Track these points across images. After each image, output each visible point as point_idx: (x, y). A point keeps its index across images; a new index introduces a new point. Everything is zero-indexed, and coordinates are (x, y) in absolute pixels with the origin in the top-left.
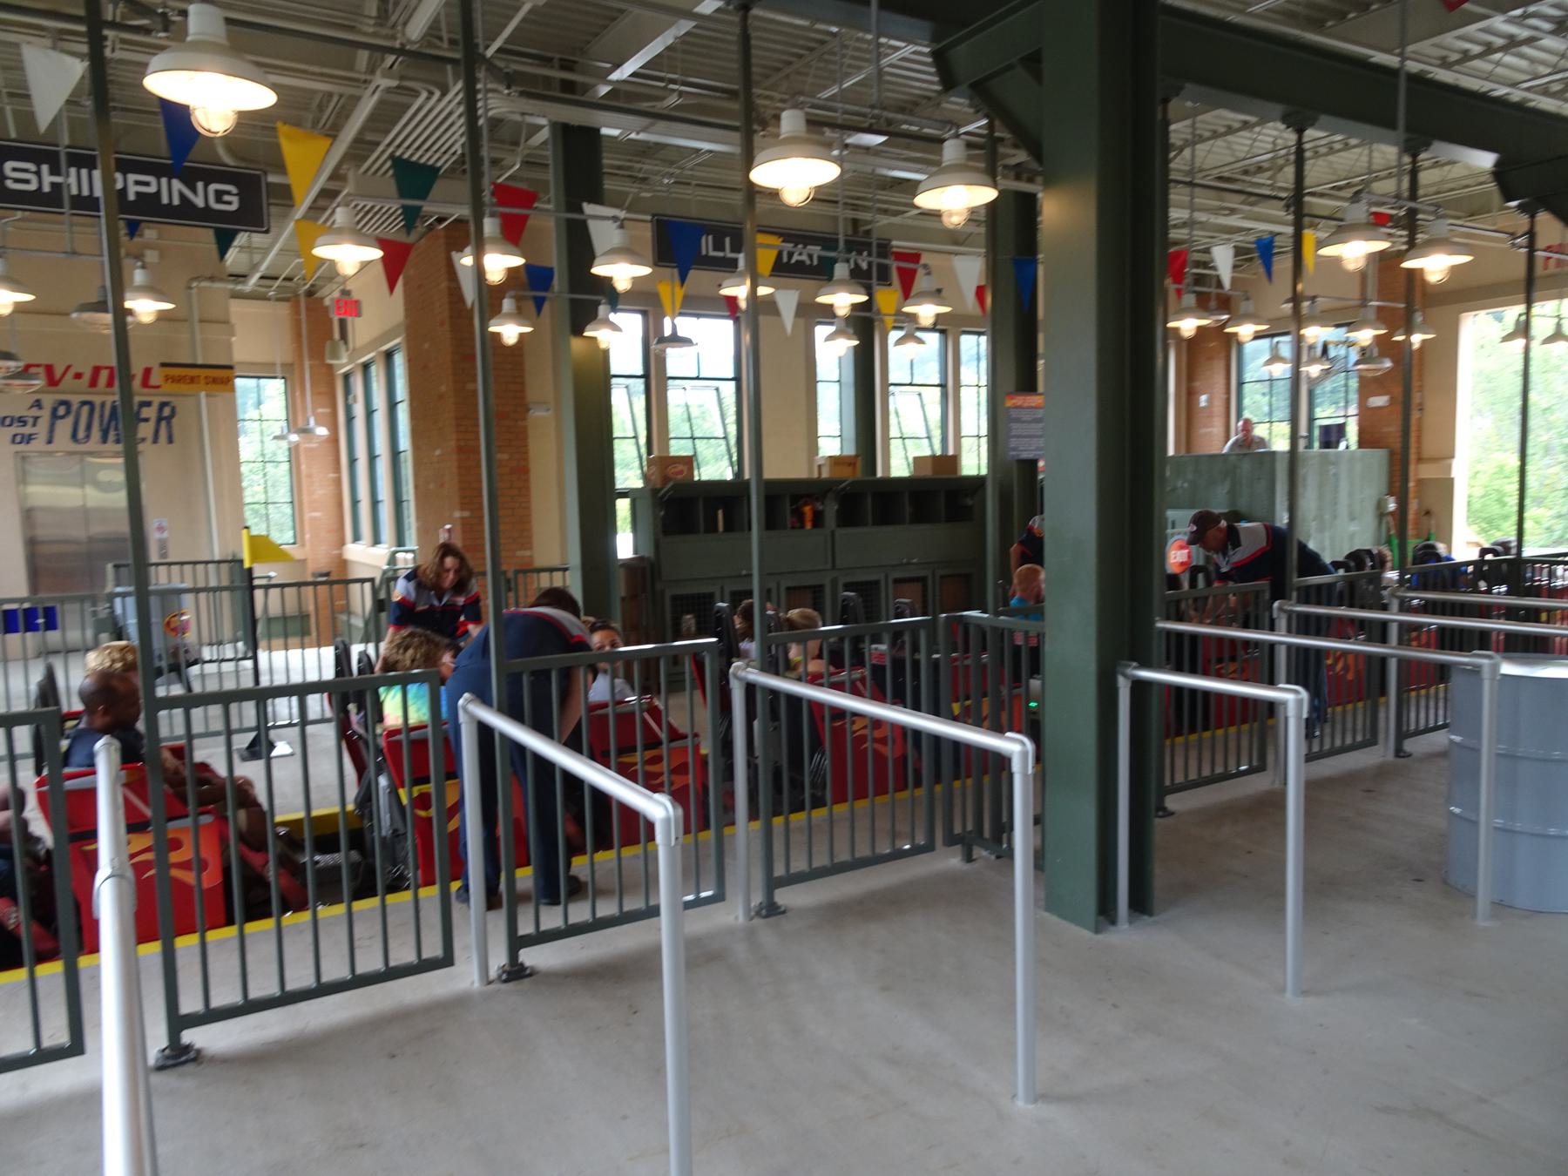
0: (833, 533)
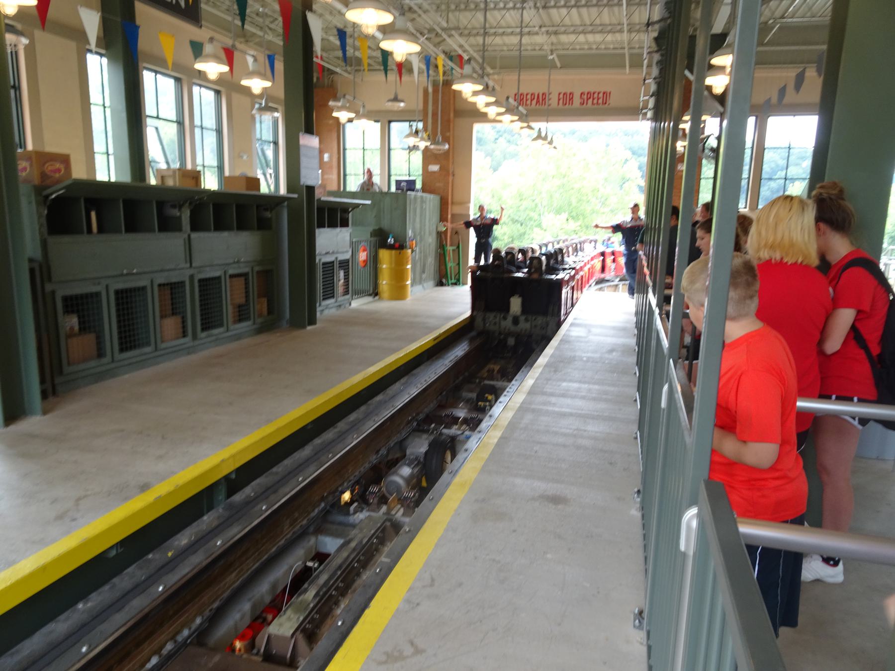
0: (189, 236)
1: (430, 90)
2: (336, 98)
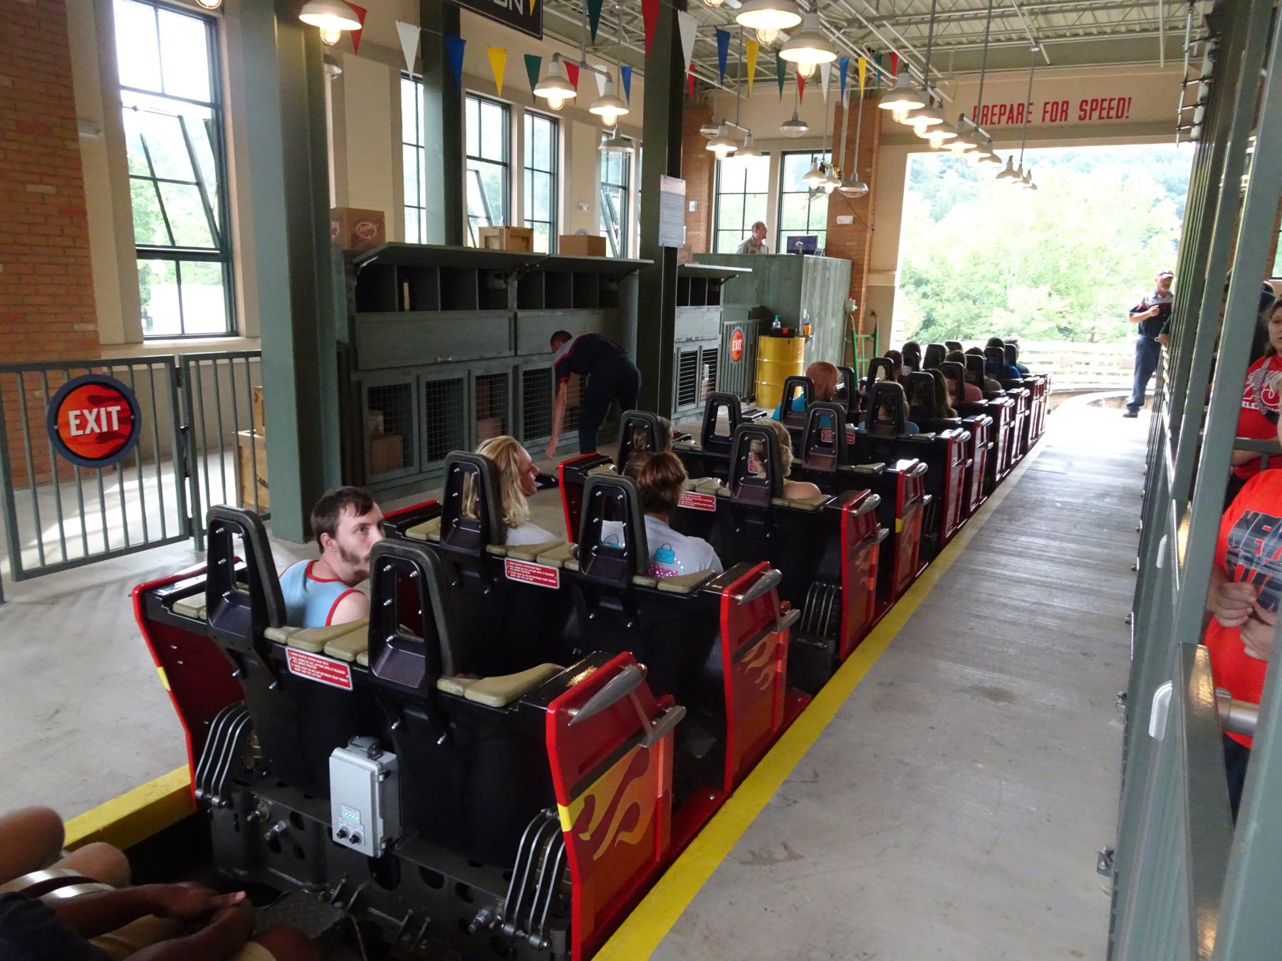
0: (516, 315)
1: (846, 105)
2: (710, 123)
